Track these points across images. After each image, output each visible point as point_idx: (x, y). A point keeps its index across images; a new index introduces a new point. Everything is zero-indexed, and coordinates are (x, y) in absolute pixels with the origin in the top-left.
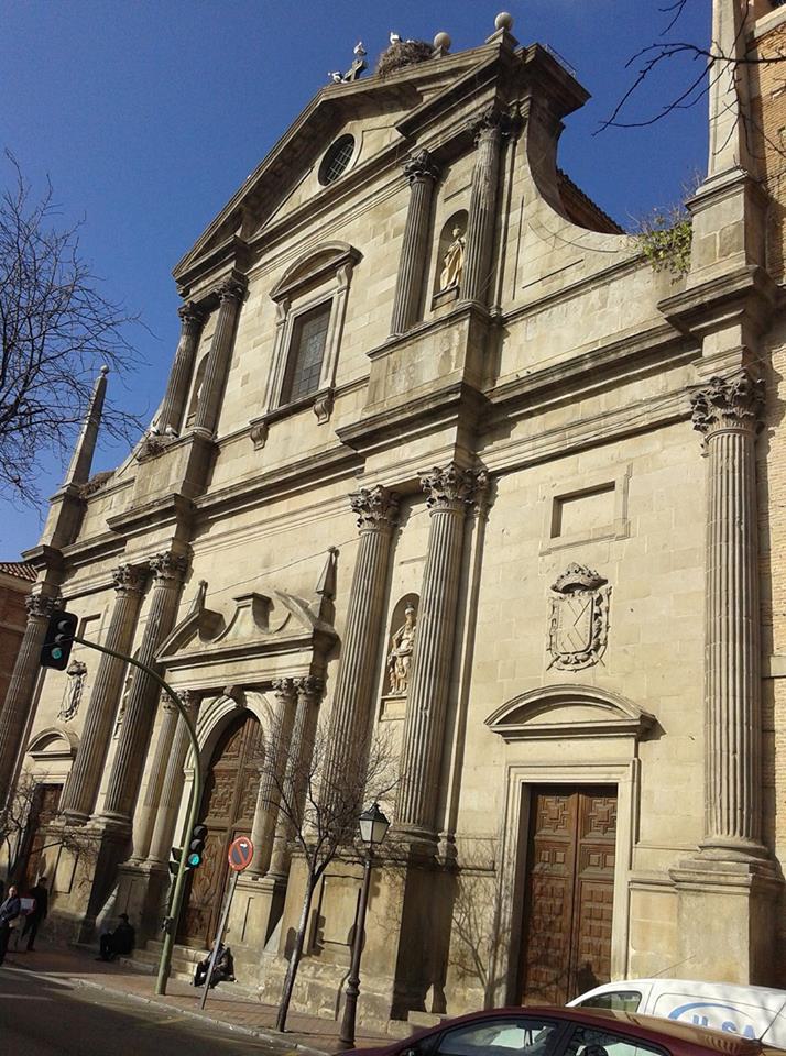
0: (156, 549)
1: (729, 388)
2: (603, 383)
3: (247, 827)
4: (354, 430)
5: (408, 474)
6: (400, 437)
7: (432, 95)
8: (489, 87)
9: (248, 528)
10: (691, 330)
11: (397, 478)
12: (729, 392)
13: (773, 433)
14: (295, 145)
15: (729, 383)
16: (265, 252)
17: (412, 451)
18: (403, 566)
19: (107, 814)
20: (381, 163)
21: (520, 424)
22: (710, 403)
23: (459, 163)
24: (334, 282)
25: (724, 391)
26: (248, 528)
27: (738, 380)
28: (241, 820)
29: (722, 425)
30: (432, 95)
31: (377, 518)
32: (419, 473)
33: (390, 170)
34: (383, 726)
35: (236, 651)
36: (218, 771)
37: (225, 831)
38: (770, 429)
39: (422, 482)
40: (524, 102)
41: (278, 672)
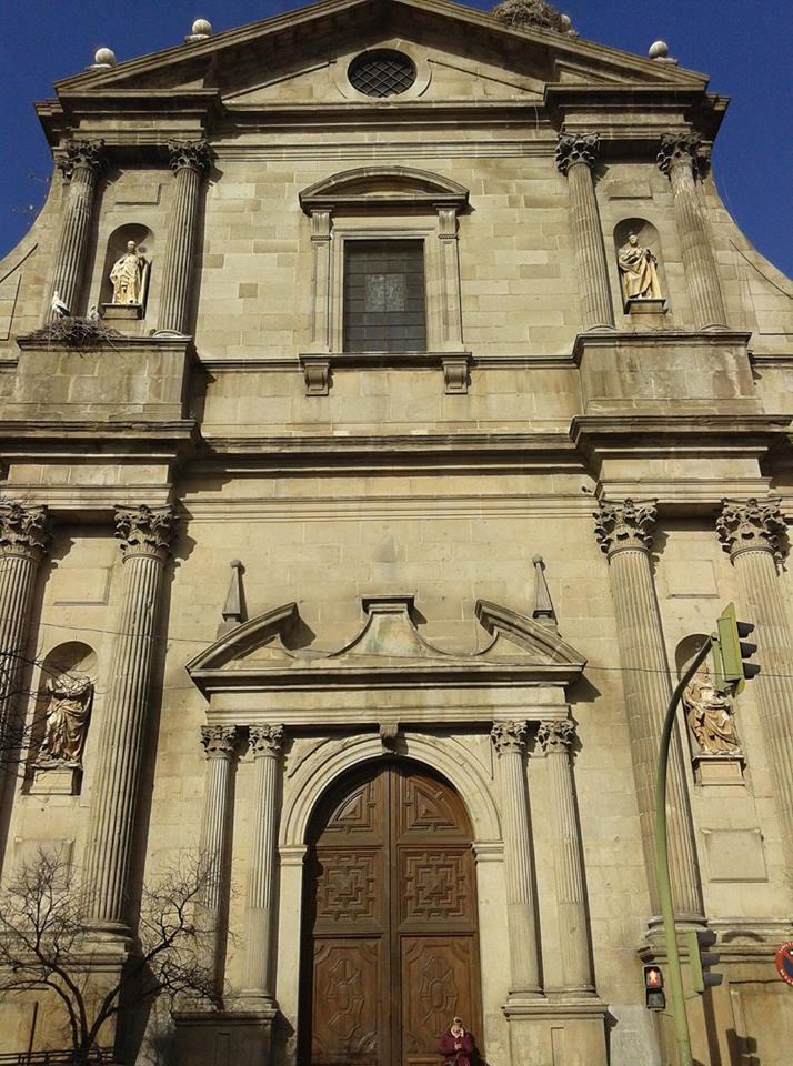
0: (116, 494)
1: (154, 517)
2: (277, 470)
3: (473, 928)
4: (609, 424)
5: (694, 496)
6: (672, 449)
7: (585, 81)
8: (677, 111)
9: (332, 500)
10: (597, 450)
11: (674, 496)
12: (153, 520)
13: (55, 565)
14: (320, 25)
15: (154, 513)
16: (252, 131)
17: (687, 470)
18: (673, 599)
19: (107, 925)
20: (363, 115)
21: (235, 482)
22: (134, 526)
23: (619, 166)
24: (432, 220)
25: (21, 520)
26: (332, 500)
27: (165, 513)
28: (406, 921)
29: (143, 548)
30: (585, 81)
31: (31, 544)
32: (117, 506)
33: (502, 126)
34: (33, 803)
35: (411, 674)
36: (323, 848)
37: (376, 937)
38: (177, 560)
39: (118, 517)
40: (705, 145)
41: (496, 710)
